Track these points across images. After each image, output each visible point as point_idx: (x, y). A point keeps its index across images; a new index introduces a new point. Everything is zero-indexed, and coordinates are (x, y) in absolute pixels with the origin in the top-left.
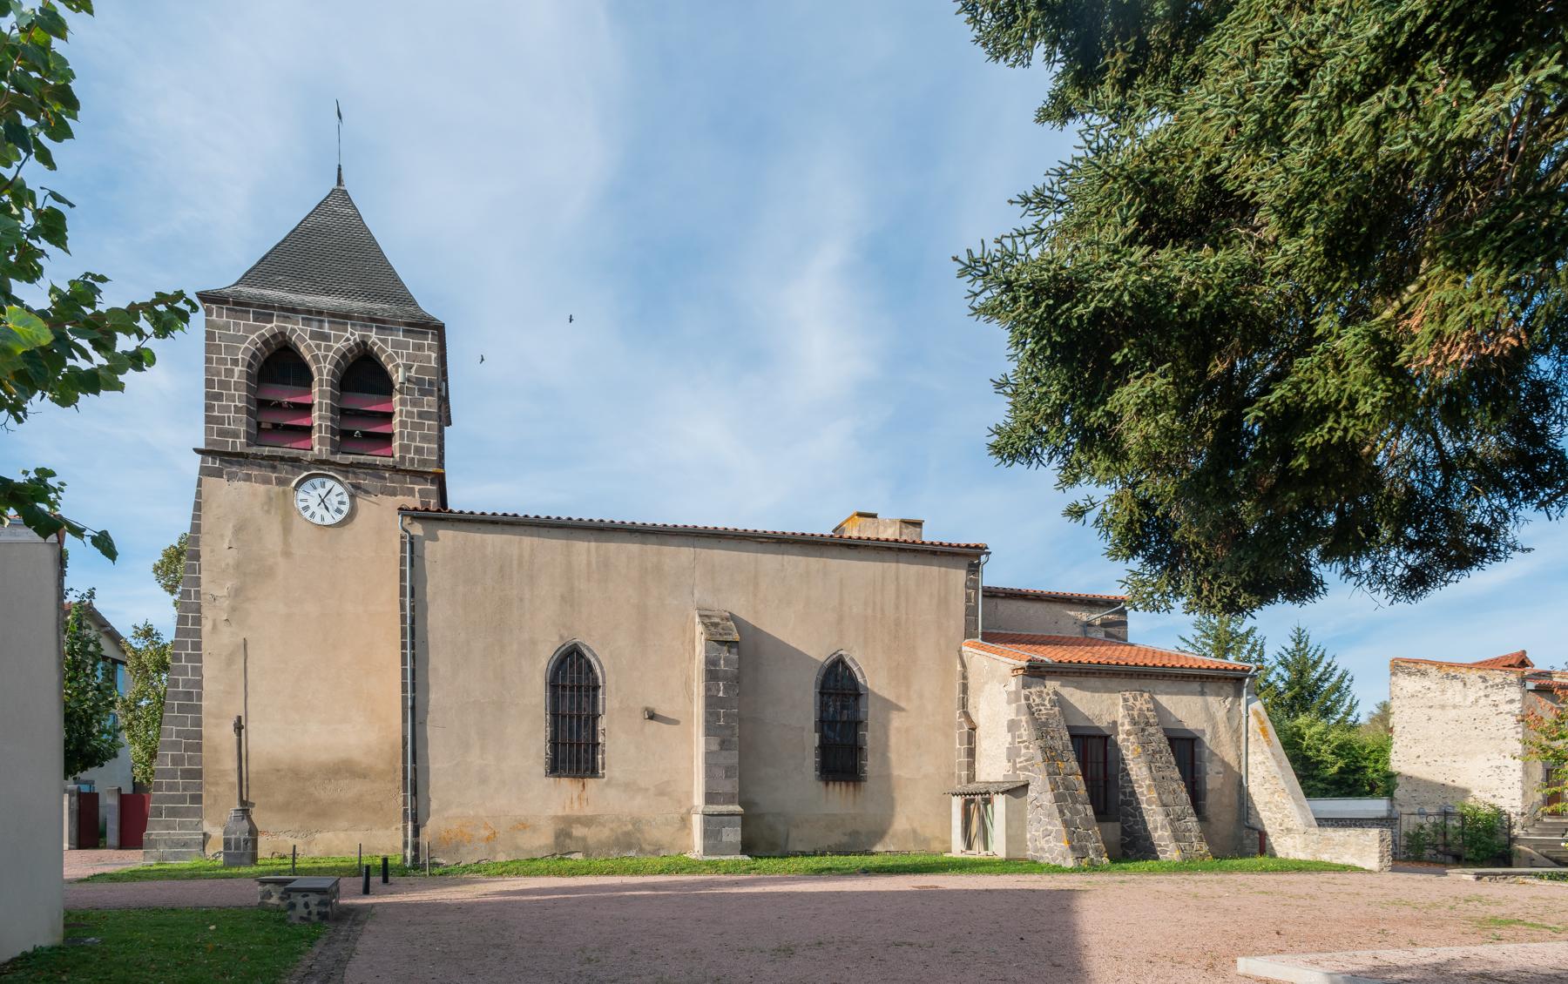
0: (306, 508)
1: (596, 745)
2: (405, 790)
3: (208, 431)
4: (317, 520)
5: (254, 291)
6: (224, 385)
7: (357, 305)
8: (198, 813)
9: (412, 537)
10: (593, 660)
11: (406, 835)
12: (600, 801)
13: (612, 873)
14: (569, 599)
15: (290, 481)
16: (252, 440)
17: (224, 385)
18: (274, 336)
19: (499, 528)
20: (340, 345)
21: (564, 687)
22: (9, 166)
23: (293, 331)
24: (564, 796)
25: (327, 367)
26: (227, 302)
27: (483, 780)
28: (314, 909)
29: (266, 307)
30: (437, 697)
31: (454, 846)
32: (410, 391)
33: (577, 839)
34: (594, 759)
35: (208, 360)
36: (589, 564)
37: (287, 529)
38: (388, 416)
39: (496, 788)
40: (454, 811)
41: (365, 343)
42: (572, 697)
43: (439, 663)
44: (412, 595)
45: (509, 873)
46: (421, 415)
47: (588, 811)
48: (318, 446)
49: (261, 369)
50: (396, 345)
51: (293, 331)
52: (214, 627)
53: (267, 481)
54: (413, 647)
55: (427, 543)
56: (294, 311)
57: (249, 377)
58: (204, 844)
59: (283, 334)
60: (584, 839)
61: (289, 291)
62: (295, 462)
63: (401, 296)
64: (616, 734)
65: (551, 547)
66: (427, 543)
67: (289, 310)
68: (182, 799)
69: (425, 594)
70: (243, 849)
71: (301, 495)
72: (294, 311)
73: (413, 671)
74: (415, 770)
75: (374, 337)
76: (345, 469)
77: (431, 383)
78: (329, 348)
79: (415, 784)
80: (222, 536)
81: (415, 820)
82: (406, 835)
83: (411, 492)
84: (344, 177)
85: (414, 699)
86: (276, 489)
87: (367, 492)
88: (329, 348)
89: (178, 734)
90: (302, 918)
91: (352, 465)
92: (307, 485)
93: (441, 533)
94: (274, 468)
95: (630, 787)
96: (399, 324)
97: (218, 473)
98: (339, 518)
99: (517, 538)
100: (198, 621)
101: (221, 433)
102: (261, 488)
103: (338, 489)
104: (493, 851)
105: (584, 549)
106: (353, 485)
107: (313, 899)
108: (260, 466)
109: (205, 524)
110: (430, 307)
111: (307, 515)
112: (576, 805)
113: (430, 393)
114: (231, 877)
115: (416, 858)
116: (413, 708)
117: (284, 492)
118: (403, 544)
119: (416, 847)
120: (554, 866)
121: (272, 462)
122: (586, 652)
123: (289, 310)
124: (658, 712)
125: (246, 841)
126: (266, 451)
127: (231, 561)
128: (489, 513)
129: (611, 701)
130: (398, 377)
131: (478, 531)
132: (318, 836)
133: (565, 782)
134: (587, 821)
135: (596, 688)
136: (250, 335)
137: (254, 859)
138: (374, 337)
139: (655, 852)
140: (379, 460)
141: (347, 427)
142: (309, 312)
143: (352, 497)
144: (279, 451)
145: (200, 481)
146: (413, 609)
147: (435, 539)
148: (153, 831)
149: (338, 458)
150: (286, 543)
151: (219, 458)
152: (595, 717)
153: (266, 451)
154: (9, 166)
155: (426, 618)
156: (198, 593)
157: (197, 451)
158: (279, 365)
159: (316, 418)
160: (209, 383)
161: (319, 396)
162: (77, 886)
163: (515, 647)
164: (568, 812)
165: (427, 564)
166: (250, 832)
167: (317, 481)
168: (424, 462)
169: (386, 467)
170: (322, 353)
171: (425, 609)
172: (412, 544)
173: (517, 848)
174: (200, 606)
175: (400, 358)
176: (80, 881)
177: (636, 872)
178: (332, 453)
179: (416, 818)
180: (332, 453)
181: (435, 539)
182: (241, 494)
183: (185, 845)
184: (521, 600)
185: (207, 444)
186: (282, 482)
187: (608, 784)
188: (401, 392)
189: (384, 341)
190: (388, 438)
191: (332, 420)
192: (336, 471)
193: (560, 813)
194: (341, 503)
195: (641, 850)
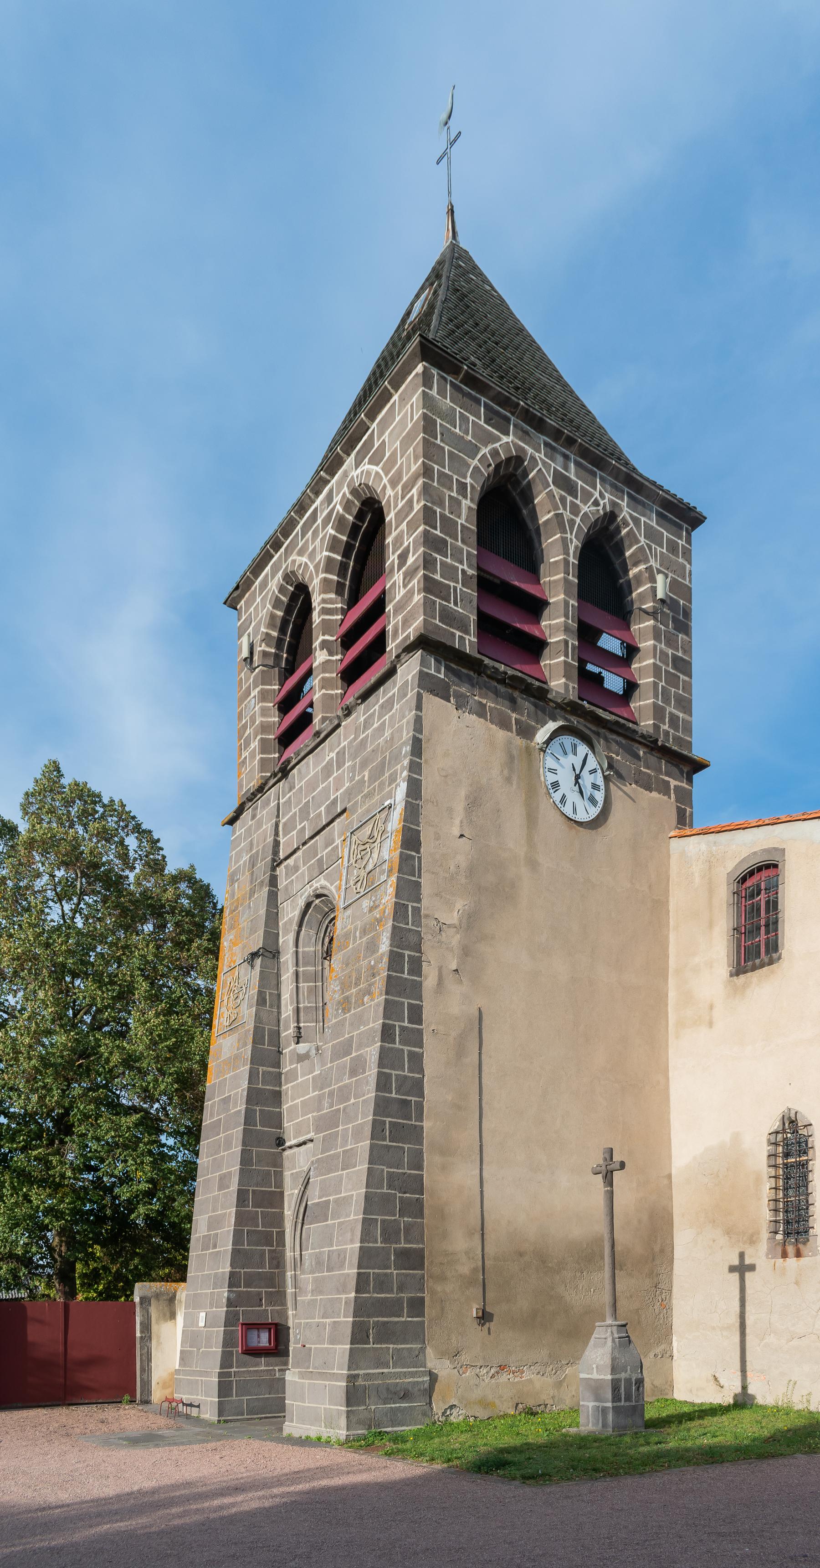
0: (556, 785)
4: (568, 810)
8: (418, 1334)
17: (449, 526)
22: (105, 1375)
53: (504, 724)
58: (429, 1392)
68: (393, 1308)
71: (550, 762)
75: (626, 512)
78: (575, 510)
80: (450, 810)
84: (457, 228)
97: (441, 691)
100: (416, 967)
117: (528, 751)
127: (462, 860)
150: (531, 842)
154: (105, 1375)
156: (417, 911)
183: (406, 1396)
189: (636, 521)
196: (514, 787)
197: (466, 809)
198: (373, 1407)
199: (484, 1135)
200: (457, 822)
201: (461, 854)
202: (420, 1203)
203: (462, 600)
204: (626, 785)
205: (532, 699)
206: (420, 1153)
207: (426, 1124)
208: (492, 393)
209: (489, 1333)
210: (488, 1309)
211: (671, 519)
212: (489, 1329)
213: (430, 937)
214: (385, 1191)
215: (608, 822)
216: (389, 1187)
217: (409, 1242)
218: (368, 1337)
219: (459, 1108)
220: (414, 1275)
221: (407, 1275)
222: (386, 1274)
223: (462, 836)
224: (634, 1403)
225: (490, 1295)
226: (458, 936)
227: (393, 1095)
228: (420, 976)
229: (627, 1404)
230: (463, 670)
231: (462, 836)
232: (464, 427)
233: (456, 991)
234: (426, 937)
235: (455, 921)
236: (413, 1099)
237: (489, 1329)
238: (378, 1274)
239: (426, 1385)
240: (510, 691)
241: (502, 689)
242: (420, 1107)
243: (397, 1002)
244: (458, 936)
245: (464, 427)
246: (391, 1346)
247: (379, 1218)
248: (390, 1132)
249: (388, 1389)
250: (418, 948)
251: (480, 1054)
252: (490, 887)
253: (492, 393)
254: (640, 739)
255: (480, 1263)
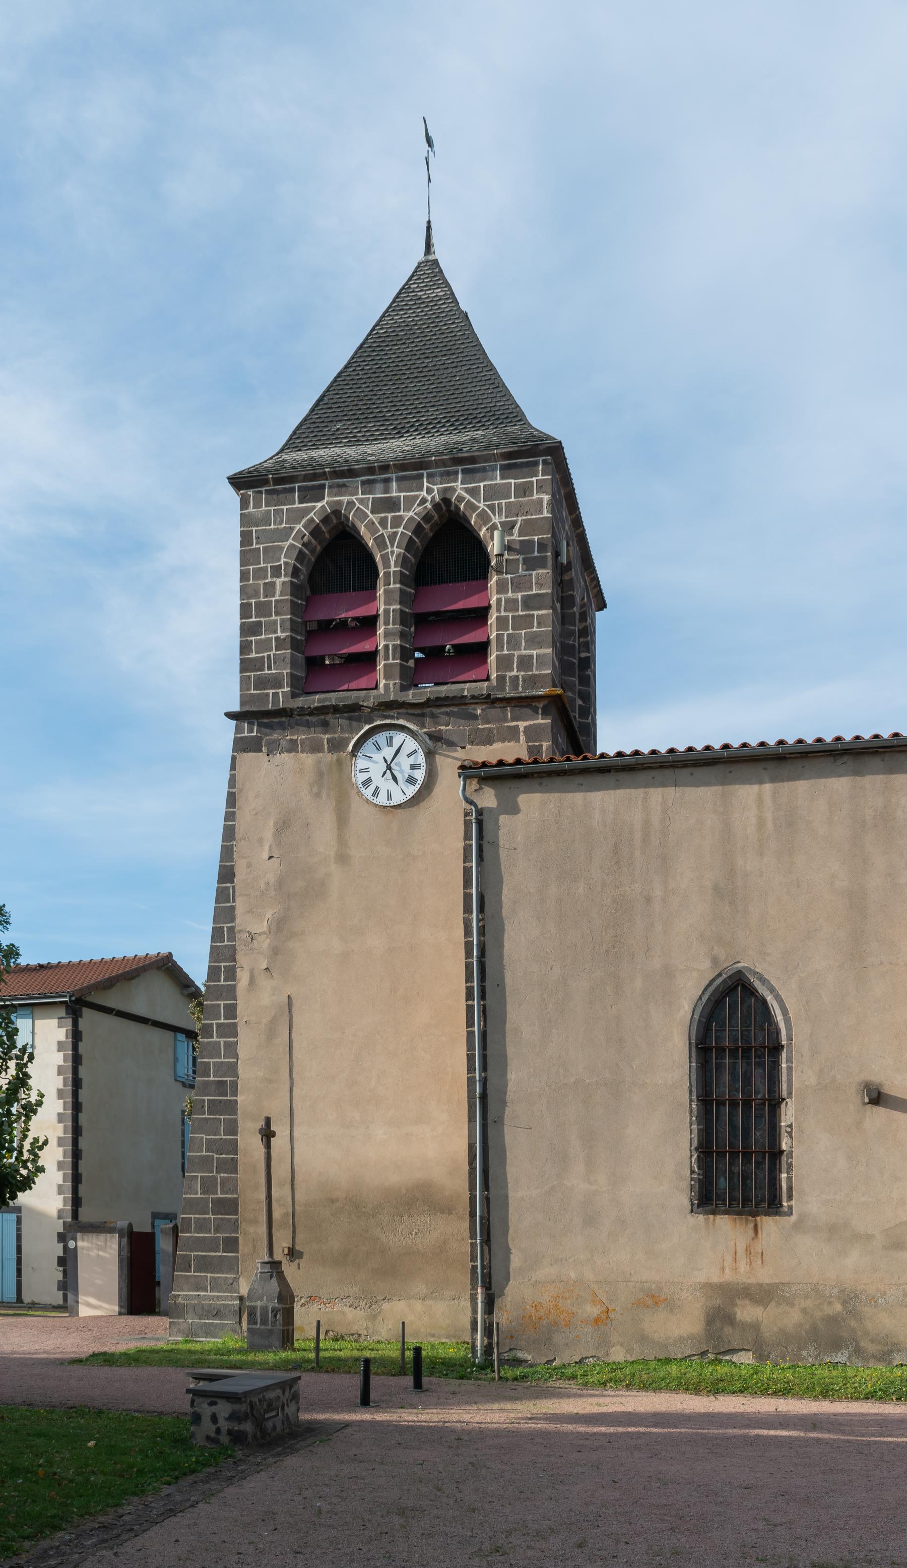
0: (367, 782)
1: (776, 1154)
2: (473, 1236)
3: (244, 683)
4: (382, 800)
5: (302, 455)
6: (264, 609)
7: (435, 442)
9: (480, 812)
10: (770, 999)
11: (474, 1311)
12: (786, 1257)
13: (785, 1392)
14: (728, 893)
15: (348, 740)
16: (300, 687)
18: (326, 520)
19: (611, 778)
20: (412, 514)
21: (721, 1050)
23: (351, 504)
24: (717, 1249)
25: (395, 551)
26: (265, 482)
27: (591, 1220)
28: (224, 1425)
29: (314, 477)
30: (520, 1076)
31: (544, 1330)
32: (511, 566)
33: (744, 1326)
34: (774, 1183)
35: (244, 576)
36: (761, 824)
37: (342, 819)
38: (480, 615)
39: (618, 1226)
40: (546, 1271)
41: (446, 501)
42: (733, 1067)
43: (521, 1018)
44: (481, 909)
45: (617, 1382)
46: (529, 602)
47: (764, 1276)
48: (384, 682)
49: (311, 577)
50: (493, 493)
51: (351, 504)
52: (252, 980)
53: (316, 748)
54: (483, 996)
55: (503, 819)
56: (351, 473)
57: (295, 590)
59: (336, 513)
60: (755, 1327)
61: (349, 444)
62: (353, 711)
63: (501, 407)
64: (813, 1134)
65: (697, 800)
66: (503, 819)
67: (344, 473)
68: (212, 1245)
69: (500, 902)
70: (276, 1321)
71: (361, 763)
72: (351, 473)
73: (484, 1036)
74: (487, 1201)
75: (459, 487)
76: (420, 711)
77: (542, 546)
78: (397, 522)
79: (488, 1224)
80: (261, 841)
81: (487, 1286)
82: (474, 1311)
83: (513, 734)
84: (435, 239)
85: (484, 1082)
86: (328, 757)
87: (451, 744)
88: (397, 522)
89: (210, 1145)
90: (208, 1438)
91: (429, 703)
92: (368, 747)
93: (523, 799)
94: (325, 725)
95: (837, 1232)
96: (494, 458)
98: (412, 790)
99: (640, 792)
100: (231, 974)
101: (261, 683)
102: (308, 759)
103: (411, 744)
104: (604, 1343)
105: (751, 798)
106: (431, 736)
107: (224, 1409)
108: (308, 725)
109: (241, 825)
110: (543, 417)
111: (368, 792)
112: (743, 1266)
113: (540, 563)
114: (252, 1365)
115: (488, 1350)
116: (484, 1096)
118: (467, 824)
119: (488, 1331)
120: (692, 1374)
121: (322, 716)
122: (757, 984)
123: (344, 473)
124: (886, 1090)
125: (275, 1311)
126: (316, 700)
127: (271, 878)
128: (754, 743)
129: (800, 1073)
130: (494, 547)
131: (580, 788)
132: (386, 1306)
133: (724, 1222)
134: (762, 1295)
135: (776, 1049)
136: (296, 521)
137: (287, 1339)
138: (459, 487)
139: (885, 1357)
140: (467, 689)
141: (433, 640)
142: (371, 470)
143: (430, 755)
144: (332, 698)
145: (234, 759)
146: (482, 931)
147: (514, 810)
148: (182, 1292)
149: (411, 696)
150: (341, 840)
151: (260, 722)
152: (775, 1103)
153: (316, 700)
155: (501, 946)
156: (231, 930)
157: (230, 715)
158: (337, 560)
159: (385, 639)
160: (245, 611)
161: (385, 602)
162: (79, 1370)
163: (639, 983)
164: (728, 1276)
165: (503, 854)
166: (281, 1298)
167: (381, 738)
168: (532, 681)
169: (477, 699)
170: (388, 530)
171: (501, 929)
172: (480, 823)
173: (643, 1339)
174: (233, 949)
175: (500, 512)
176: (61, 1362)
177: (826, 1393)
178: (404, 688)
179: (490, 1283)
180: (404, 688)
181: (514, 810)
182: (284, 772)
183: (218, 1314)
184: (648, 900)
185: (242, 703)
186: (336, 746)
187: (798, 1226)
188: (499, 572)
189: (473, 492)
190: (480, 650)
191: (403, 635)
192: (410, 717)
193: (715, 1279)
194: (414, 767)
195: (858, 1352)
196: (324, 798)
197: (274, 834)
198: (190, 1321)
199: (295, 1101)
200: (267, 848)
201: (270, 872)
202: (234, 1162)
203: (275, 663)
204: (456, 751)
205: (346, 715)
206: (235, 1121)
207: (240, 1098)
208: (300, 478)
209: (299, 1268)
210: (297, 1248)
211: (521, 463)
212: (299, 1265)
213: (243, 947)
214: (204, 1153)
215: (433, 794)
216: (208, 1151)
217: (226, 1193)
218: (190, 1267)
219: (270, 1081)
220: (229, 1220)
221: (223, 1219)
222: (205, 1219)
223: (270, 857)
224: (270, 1327)
225: (300, 1237)
226: (268, 940)
227: (211, 1078)
228: (235, 980)
229: (263, 1327)
230: (275, 720)
231: (270, 857)
232: (278, 520)
233: (265, 984)
234: (239, 947)
235: (265, 929)
236: (228, 1079)
237: (299, 1265)
238: (199, 1219)
239: (237, 1308)
240: (322, 717)
241: (313, 719)
242: (234, 1085)
243: (214, 1005)
244: (268, 940)
245: (278, 520)
246: (209, 1275)
247: (199, 1175)
248: (209, 1107)
249: (203, 1308)
250: (233, 958)
251: (290, 1034)
252: (300, 893)
253: (300, 478)
254: (472, 701)
255: (290, 1210)
